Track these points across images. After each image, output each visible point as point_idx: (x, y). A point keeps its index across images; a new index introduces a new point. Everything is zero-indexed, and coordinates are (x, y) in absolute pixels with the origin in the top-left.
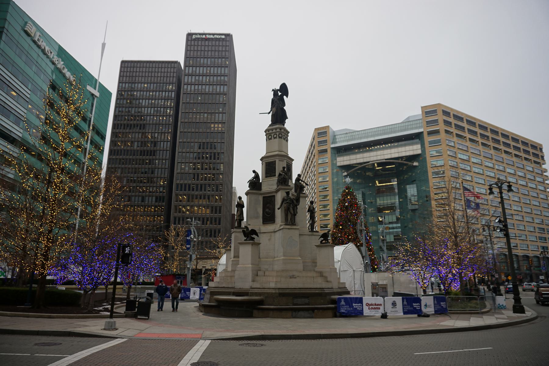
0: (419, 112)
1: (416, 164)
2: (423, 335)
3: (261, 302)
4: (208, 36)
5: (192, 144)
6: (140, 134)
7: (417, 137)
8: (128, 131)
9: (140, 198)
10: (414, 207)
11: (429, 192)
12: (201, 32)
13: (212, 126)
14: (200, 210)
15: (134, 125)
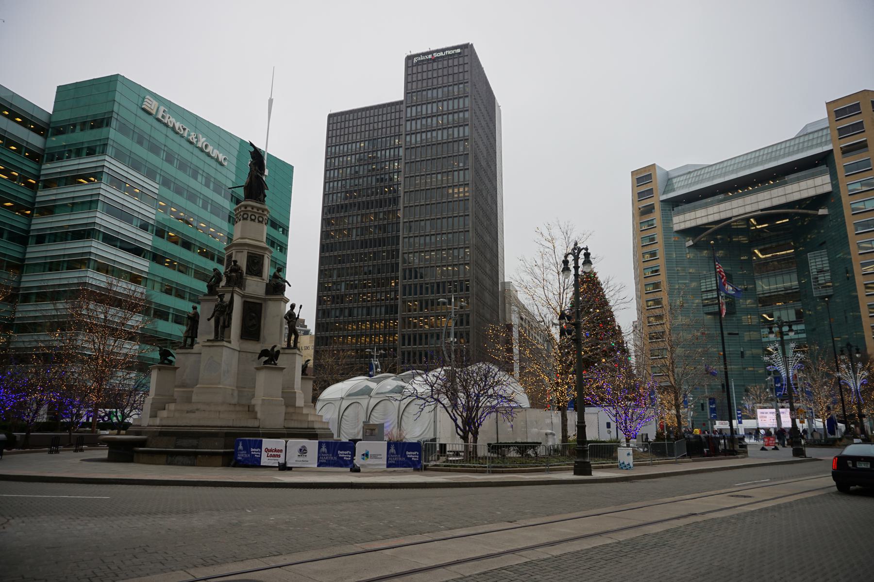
0: (822, 114)
1: (822, 212)
2: (124, 486)
3: (143, 443)
4: (435, 55)
5: (423, 223)
6: (359, 217)
7: (823, 161)
8: (342, 214)
9: (383, 309)
10: (824, 292)
11: (850, 261)
12: (426, 50)
13: (450, 191)
14: (439, 322)
15: (351, 204)
